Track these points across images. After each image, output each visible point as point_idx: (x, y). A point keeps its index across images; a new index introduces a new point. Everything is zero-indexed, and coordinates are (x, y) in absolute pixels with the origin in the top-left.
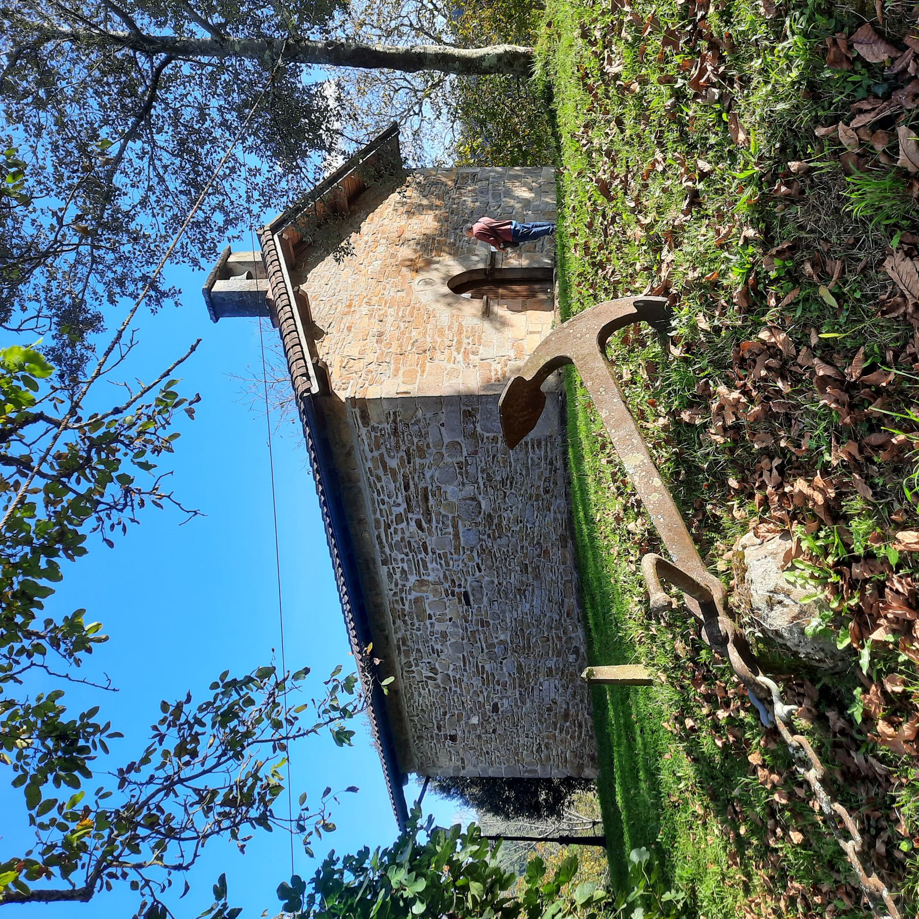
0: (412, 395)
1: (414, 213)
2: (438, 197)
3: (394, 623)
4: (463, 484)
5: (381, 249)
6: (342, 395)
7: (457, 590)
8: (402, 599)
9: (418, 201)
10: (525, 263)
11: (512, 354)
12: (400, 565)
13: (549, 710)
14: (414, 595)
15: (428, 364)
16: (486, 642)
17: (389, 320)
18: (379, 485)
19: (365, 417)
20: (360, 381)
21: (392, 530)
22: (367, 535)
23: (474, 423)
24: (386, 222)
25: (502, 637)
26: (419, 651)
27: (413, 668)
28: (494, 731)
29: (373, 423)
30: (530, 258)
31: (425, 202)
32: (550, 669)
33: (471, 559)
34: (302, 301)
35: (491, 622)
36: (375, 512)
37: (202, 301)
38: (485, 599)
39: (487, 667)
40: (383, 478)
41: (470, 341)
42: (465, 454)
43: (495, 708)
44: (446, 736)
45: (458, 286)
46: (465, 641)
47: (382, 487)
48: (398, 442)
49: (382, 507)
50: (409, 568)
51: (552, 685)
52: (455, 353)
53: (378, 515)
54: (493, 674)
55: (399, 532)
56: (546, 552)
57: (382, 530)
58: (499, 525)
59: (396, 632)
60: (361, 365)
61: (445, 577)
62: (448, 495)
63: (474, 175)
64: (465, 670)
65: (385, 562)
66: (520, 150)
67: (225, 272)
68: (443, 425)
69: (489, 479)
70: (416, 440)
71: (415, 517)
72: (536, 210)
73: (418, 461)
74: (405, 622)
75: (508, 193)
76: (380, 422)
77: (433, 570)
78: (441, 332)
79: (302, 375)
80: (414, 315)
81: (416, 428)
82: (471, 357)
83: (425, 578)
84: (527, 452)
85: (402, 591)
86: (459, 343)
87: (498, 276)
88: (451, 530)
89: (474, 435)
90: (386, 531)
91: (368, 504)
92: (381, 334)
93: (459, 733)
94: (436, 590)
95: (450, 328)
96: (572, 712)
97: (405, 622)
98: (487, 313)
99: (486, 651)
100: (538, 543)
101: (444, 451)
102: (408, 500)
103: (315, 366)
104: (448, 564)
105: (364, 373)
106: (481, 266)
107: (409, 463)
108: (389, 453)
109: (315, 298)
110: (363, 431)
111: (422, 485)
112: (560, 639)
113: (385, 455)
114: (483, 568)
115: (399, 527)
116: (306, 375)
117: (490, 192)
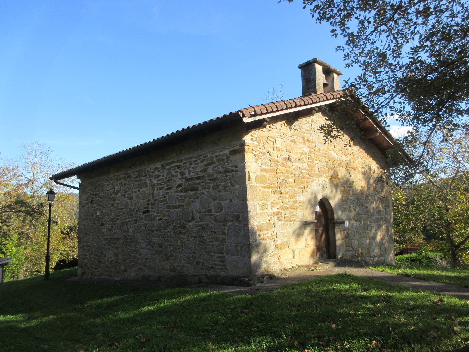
0: (248, 182)
1: (365, 175)
2: (375, 188)
3: (137, 171)
4: (200, 212)
5: (344, 158)
6: (247, 139)
7: (150, 206)
8: (146, 175)
9: (372, 177)
10: (338, 243)
11: (279, 242)
12: (161, 174)
13: (102, 253)
14: (148, 182)
15: (270, 190)
16: (129, 221)
17: (300, 165)
18: (199, 161)
19: (234, 152)
20: (258, 149)
21: (177, 170)
22: (175, 155)
23: (233, 221)
24: (360, 160)
25: (130, 230)
26: (125, 184)
27: (118, 182)
28: (94, 223)
29: (231, 158)
30: (341, 245)
31: (371, 181)
32: (117, 255)
33: (164, 215)
34: (309, 113)
35: (137, 225)
36: (185, 159)
37: (310, 59)
38: (146, 222)
39: (118, 221)
40: (203, 164)
41: (287, 215)
42: (216, 214)
43: (103, 225)
44: (93, 198)
45: (324, 203)
46: (129, 210)
47: (198, 163)
48: (221, 173)
49: (188, 164)
50: (160, 180)
51: (111, 256)
52: (278, 206)
53: (184, 161)
54: (116, 224)
55: (176, 174)
56: (168, 259)
57: (177, 164)
58: (180, 233)
59: (132, 172)
60: (269, 149)
61: (156, 200)
62: (195, 203)
63: (388, 206)
64: (117, 209)
65: (162, 166)
66: (400, 223)
67: (328, 72)
68: (231, 201)
69: (203, 229)
70: (222, 184)
71: (183, 183)
72: (370, 244)
73: (211, 185)
74: (137, 177)
75: (379, 227)
76: (232, 162)
77: (159, 193)
78: (291, 197)
79: (255, 111)
80: (303, 181)
81: (229, 184)
82: (276, 217)
83: (156, 189)
84: (218, 253)
85: (150, 175)
86: (286, 208)
87: (330, 226)
88: (178, 204)
89: (226, 221)
90: (176, 166)
91: (189, 156)
92: (290, 160)
93: (94, 205)
94: (150, 195)
95: (295, 202)
96: (101, 265)
97: (137, 177)
98: (305, 224)
99: (125, 221)
100: (172, 255)
101: (217, 201)
102: (191, 179)
103: (264, 120)
104: (162, 201)
105: (260, 153)
106: (335, 217)
107: (211, 180)
108: (215, 167)
109: (313, 121)
110: (227, 151)
111: (200, 188)
112: (130, 262)
113: (215, 165)
114: (160, 222)
115: (179, 174)
116: (255, 115)
117: (379, 217)
